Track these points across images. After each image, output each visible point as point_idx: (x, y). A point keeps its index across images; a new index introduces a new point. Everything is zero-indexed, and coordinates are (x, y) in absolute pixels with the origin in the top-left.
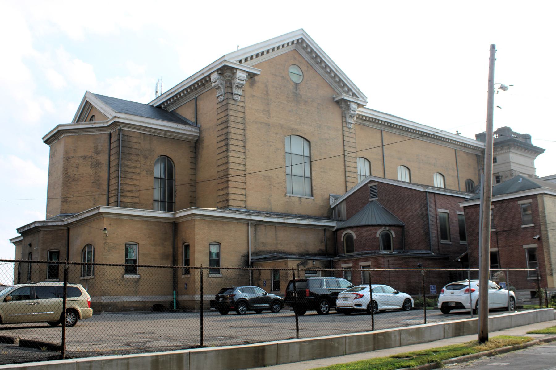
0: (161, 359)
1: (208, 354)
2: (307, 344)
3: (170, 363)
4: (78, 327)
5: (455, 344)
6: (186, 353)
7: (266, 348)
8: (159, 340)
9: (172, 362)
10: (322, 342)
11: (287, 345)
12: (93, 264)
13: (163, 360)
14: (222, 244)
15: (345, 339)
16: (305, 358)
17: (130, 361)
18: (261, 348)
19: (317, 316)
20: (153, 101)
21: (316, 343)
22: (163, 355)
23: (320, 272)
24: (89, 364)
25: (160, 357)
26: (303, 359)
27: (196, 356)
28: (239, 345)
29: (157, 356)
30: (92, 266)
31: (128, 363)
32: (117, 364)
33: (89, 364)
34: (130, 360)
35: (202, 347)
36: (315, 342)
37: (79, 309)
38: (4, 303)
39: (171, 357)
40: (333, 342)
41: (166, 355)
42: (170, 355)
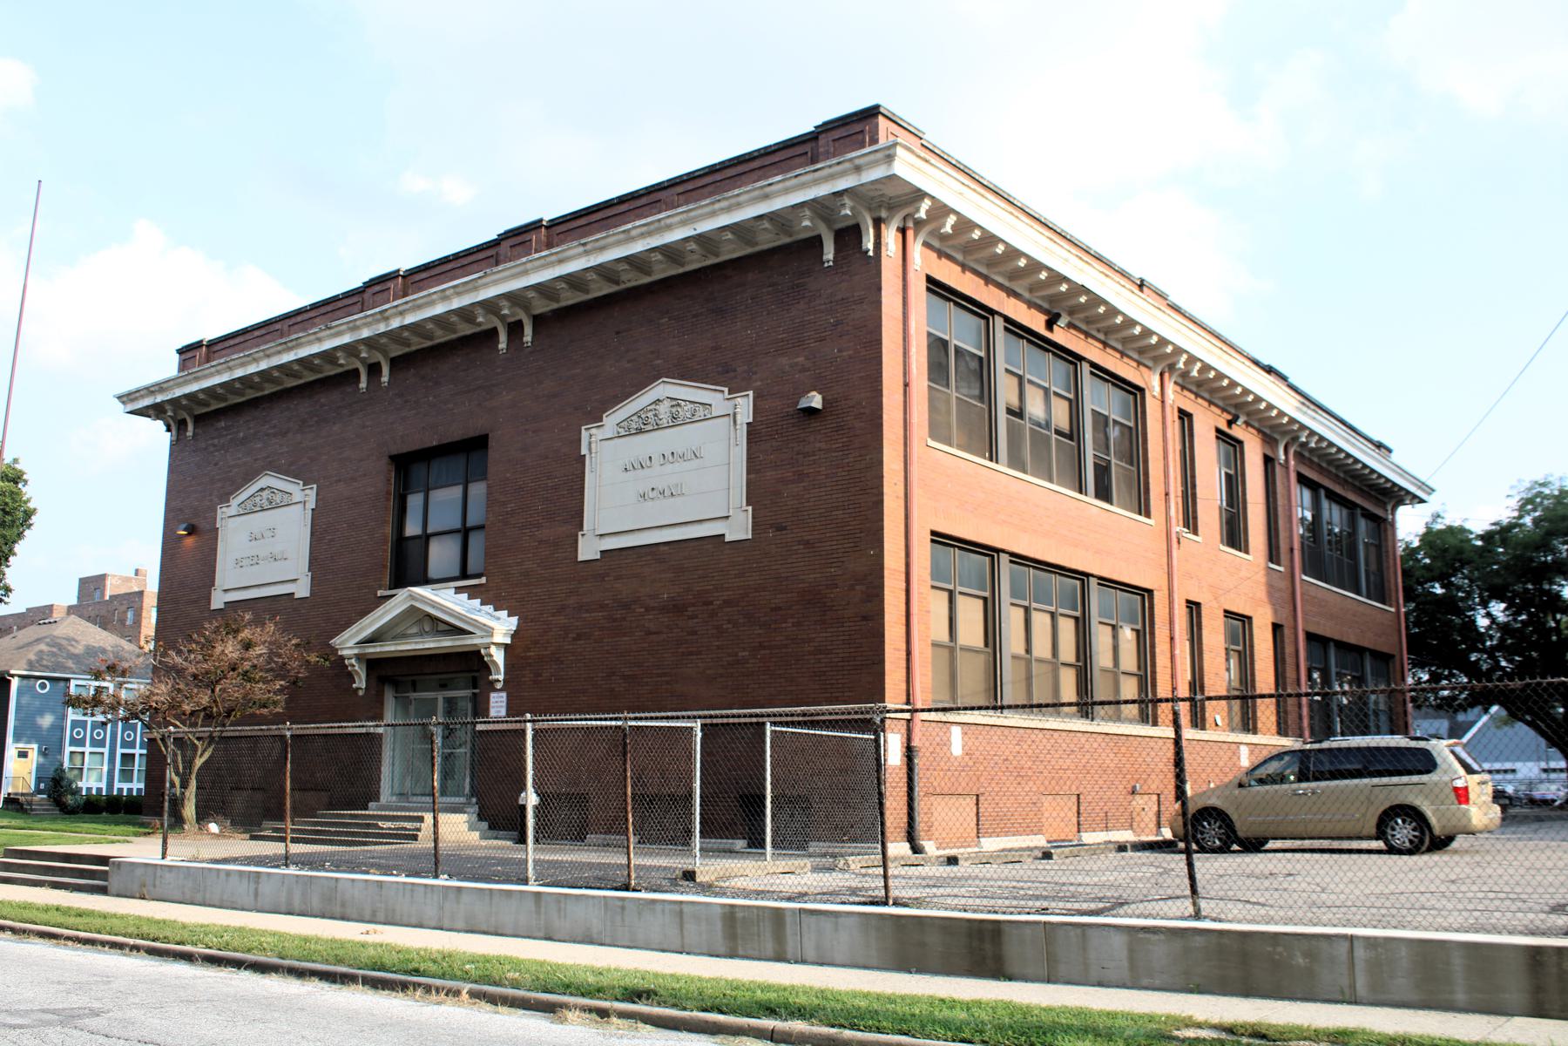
0: (740, 915)
1: (841, 920)
2: (1162, 937)
3: (759, 926)
4: (1457, 858)
5: (217, 974)
6: (793, 910)
7: (1006, 928)
8: (948, 877)
9: (761, 924)
10: (1225, 941)
11: (1079, 931)
12: (1151, 701)
13: (744, 918)
14: (1255, 622)
15: (1346, 944)
16: (1157, 982)
17: (686, 908)
18: (990, 927)
19: (1387, 856)
20: (519, 240)
21: (1199, 941)
22: (744, 906)
23: (16, 678)
24: (620, 903)
25: (737, 910)
26: (1145, 982)
27: (813, 918)
28: (1543, 934)
29: (732, 906)
30: (1150, 705)
31: (681, 912)
32: (663, 911)
33: (620, 903)
34: (684, 906)
35: (886, 904)
36: (1198, 938)
37: (1428, 811)
38: (1237, 792)
39: (761, 913)
40: (1280, 949)
41: (749, 907)
42: (758, 908)
